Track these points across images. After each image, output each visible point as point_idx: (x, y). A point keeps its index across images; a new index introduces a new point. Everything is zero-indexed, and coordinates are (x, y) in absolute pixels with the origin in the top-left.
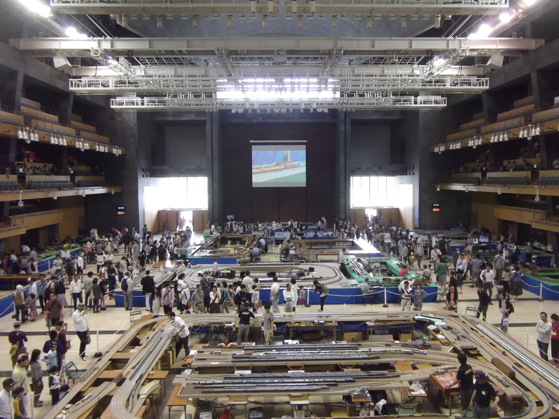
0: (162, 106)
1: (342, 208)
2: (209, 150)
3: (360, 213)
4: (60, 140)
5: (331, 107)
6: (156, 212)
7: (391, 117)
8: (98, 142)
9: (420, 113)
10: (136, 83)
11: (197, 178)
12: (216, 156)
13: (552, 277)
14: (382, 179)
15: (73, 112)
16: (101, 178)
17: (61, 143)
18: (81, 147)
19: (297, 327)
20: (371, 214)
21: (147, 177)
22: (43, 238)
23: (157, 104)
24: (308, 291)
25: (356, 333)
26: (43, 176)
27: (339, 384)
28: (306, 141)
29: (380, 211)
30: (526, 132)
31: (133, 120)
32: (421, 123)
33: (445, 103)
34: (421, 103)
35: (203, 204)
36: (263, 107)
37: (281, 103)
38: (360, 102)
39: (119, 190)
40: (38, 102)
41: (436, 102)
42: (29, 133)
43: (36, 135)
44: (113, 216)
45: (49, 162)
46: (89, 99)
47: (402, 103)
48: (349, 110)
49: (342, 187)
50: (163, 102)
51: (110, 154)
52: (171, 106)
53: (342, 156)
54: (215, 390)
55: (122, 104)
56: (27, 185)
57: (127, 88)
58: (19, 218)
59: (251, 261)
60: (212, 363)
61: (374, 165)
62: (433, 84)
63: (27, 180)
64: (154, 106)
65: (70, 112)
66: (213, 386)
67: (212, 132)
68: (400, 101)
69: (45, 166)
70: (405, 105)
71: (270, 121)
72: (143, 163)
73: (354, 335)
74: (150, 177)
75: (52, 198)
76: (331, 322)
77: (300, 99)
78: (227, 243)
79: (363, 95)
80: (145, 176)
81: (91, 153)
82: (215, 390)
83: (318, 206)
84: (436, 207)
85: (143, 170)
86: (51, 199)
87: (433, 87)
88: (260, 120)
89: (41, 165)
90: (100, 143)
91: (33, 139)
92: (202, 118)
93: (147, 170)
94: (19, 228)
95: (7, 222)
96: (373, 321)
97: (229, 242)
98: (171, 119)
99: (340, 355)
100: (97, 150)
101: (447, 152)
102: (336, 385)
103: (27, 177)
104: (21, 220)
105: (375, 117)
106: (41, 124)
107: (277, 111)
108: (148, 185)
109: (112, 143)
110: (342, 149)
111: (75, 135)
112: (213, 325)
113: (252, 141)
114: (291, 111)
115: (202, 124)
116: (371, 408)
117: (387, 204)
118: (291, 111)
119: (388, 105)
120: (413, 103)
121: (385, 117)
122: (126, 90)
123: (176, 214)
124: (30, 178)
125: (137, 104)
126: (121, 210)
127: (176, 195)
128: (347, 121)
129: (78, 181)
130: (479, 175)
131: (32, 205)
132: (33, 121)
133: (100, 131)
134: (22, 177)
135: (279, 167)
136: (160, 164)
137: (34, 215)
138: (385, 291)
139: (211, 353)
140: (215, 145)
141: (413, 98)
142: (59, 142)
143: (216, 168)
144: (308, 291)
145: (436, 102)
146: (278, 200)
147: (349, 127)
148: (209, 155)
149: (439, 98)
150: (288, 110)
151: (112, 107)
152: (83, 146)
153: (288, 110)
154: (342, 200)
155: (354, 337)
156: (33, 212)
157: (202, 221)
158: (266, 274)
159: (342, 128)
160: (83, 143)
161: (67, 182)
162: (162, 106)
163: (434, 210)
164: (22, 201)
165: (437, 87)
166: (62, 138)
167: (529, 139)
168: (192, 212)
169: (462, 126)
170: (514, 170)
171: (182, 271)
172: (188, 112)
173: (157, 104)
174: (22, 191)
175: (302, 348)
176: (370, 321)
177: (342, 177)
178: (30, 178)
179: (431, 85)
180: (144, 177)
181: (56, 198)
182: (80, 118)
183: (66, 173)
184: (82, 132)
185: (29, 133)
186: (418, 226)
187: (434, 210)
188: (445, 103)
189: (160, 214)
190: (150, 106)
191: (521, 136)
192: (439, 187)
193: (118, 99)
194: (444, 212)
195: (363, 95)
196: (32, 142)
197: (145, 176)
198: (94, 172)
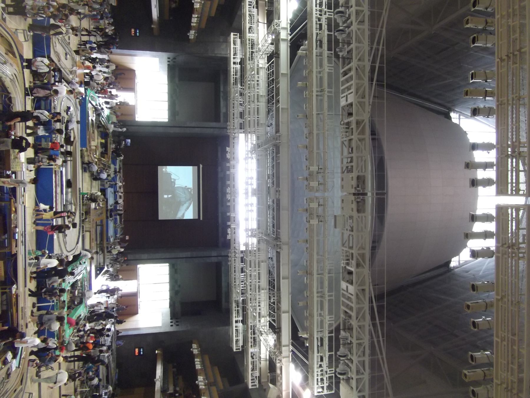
0: (232, 81)
1: (137, 256)
2: (193, 124)
5: (232, 242)
7: (223, 300)
8: (201, 17)
12: (188, 131)
19: (10, 209)
28: (201, 219)
32: (218, 328)
34: (236, 327)
39: (156, 32)
41: (237, 341)
46: (238, 13)
50: (236, 83)
51: (189, 28)
52: (232, 90)
55: (235, 44)
62: (253, 336)
64: (232, 73)
68: (238, 307)
70: (234, 312)
72: (181, 58)
74: (168, 65)
76: (16, 246)
80: (169, 60)
83: (142, 233)
84: (139, 352)
85: (175, 58)
90: (200, 18)
93: (174, 62)
97: (103, 141)
98: (222, 89)
100: (193, 16)
101: (192, 357)
105: (224, 284)
108: (160, 62)
109: (200, 31)
110: (195, 254)
113: (201, 166)
120: (237, 319)
123: (130, 87)
126: (135, 33)
127: (149, 90)
128: (220, 258)
133: (210, 20)
136: (180, 76)
141: (240, 319)
143: (177, 130)
145: (237, 341)
146: (143, 190)
147: (214, 260)
148: (188, 124)
149: (241, 343)
151: (232, 34)
154: (145, 256)
158: (69, 178)
159: (214, 253)
163: (137, 350)
165: (250, 340)
168: (134, 104)
172: (227, 106)
176: (17, 289)
177: (168, 255)
180: (169, 58)
186: (120, 334)
187: (137, 350)
190: (232, 70)
193: (238, 41)
197: (169, 60)
198: (172, 11)
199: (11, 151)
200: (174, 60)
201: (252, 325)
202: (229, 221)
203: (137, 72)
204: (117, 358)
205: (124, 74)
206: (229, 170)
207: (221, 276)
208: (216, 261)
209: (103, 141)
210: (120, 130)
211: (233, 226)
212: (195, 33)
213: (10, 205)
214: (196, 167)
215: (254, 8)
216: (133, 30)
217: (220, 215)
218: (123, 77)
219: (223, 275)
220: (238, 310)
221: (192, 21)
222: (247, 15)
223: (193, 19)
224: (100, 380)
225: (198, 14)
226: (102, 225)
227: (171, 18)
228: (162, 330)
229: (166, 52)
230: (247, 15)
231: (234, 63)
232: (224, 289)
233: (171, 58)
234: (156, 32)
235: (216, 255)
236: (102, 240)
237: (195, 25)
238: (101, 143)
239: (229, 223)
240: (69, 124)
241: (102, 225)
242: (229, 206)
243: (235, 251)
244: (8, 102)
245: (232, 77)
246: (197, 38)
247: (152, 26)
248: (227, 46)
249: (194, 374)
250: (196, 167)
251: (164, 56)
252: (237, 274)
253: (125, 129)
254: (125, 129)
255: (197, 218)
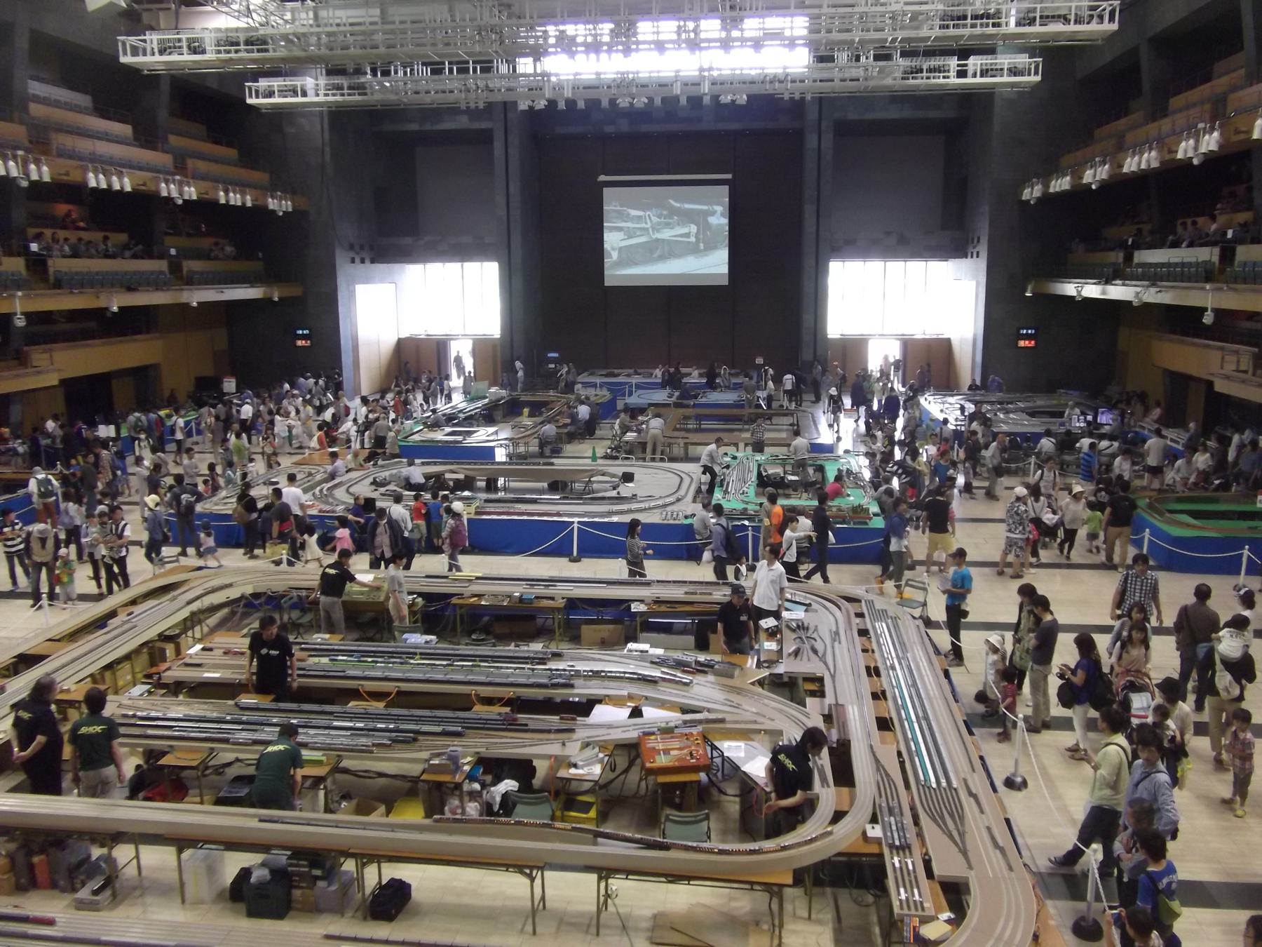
0: (357, 98)
1: (806, 337)
2: (501, 199)
3: (853, 348)
4: (115, 178)
5: (756, 90)
6: (395, 340)
7: (933, 114)
8: (224, 182)
9: (998, 103)
10: (265, 42)
11: (847, 264)
12: (516, 214)
13: (1196, 515)
14: (916, 267)
15: (172, 114)
16: (256, 266)
17: (117, 187)
18: (175, 194)
19: (472, 606)
20: (880, 355)
21: (363, 261)
22: (122, 392)
23: (346, 91)
24: (576, 525)
25: (611, 627)
26: (100, 261)
27: (420, 738)
28: (729, 176)
29: (908, 345)
30: (1191, 142)
31: (318, 134)
32: (997, 128)
33: (1036, 73)
34: (975, 75)
35: (490, 323)
36: (592, 95)
37: (624, 84)
38: (825, 75)
39: (293, 291)
40: (86, 93)
41: (1014, 71)
42: (25, 164)
43: (45, 169)
44: (286, 344)
45: (118, 229)
46: (213, 84)
47: (925, 74)
48: (797, 96)
49: (807, 287)
50: (361, 88)
51: (260, 211)
52: (378, 97)
53: (809, 210)
54: (150, 732)
55: (270, 94)
56: (52, 279)
57: (243, 55)
58: (45, 352)
59: (542, 455)
60: (206, 675)
61: (888, 234)
62: (969, 21)
63: (51, 270)
64: (338, 98)
65: (163, 114)
66: (132, 721)
67: (507, 153)
68: (921, 71)
69: (106, 238)
70: (933, 81)
71: (645, 128)
72: (347, 230)
73: (606, 630)
74: (372, 262)
75: (187, 304)
76: (552, 599)
77: (598, 74)
78: (521, 414)
79: (831, 59)
80: (357, 260)
81: (204, 209)
82: (150, 732)
83: (755, 329)
84: (1027, 337)
85: (352, 247)
86: (186, 306)
87: (967, 32)
88: (624, 126)
89: (96, 236)
90: (228, 184)
91: (35, 177)
92: (484, 125)
93: (362, 247)
94: (39, 373)
95: (21, 360)
96: (649, 600)
97: (526, 411)
98: (414, 127)
99: (529, 677)
100: (223, 201)
101: (1047, 200)
102: (415, 740)
103: (50, 262)
104: (46, 356)
105: (894, 113)
106: (69, 142)
107: (623, 103)
108: (367, 281)
109: (277, 185)
110: (809, 193)
111: (172, 170)
112: (295, 593)
113: (602, 178)
114: (658, 102)
115: (485, 138)
116: (473, 795)
117: (926, 328)
118: (658, 102)
119: (889, 81)
120: (953, 74)
121: (920, 114)
122: (231, 59)
123: (440, 347)
124: (58, 264)
125: (304, 94)
126: (304, 337)
127: (433, 302)
128: (824, 124)
129: (189, 271)
130: (1119, 256)
131: (92, 325)
132: (53, 136)
133: (249, 159)
134: (37, 265)
135: (666, 239)
136: (396, 234)
137: (1197, 345)
138: (750, 533)
139: (225, 653)
140: (514, 189)
141: (953, 62)
142: (110, 185)
144: (576, 525)
145: (1014, 71)
147: (828, 141)
148: (502, 212)
149: (1023, 60)
150: (651, 100)
151: (249, 101)
152: (181, 194)
153: (651, 100)
154: (807, 318)
155: (605, 635)
156: (84, 339)
157: (495, 360)
158: (545, 485)
159: (811, 141)
160: (181, 185)
161: (162, 273)
162: (357, 98)
163: (1022, 343)
164: (22, 314)
165: (978, 30)
166: (121, 175)
167: (1195, 162)
168: (471, 342)
169: (1097, 132)
170: (1191, 245)
171: (988, 470)
172: (453, 111)
173: (346, 91)
174: (20, 294)
175: (415, 654)
176: (642, 601)
177: (809, 262)
178: (58, 264)
179: (965, 26)
180: (353, 261)
181: (195, 304)
182: (200, 129)
183: (162, 255)
184: (190, 163)
185: (25, 164)
186: (978, 383)
187: (1022, 343)
188: (1036, 73)
189: (402, 346)
190: (330, 98)
191: (1180, 156)
192: (1030, 288)
193: (263, 83)
194: (1041, 348)
195: (831, 59)
196: (33, 183)
197: (357, 260)
198: (244, 252)
199: (344, 598)
200: (357, 248)
201: (938, 22)
202: (598, 102)
203: (404, 334)
204: (1023, 392)
205: (406, 363)
206: (676, 99)
207: (873, 122)
208: (831, 136)
209: (526, 411)
210: (520, 374)
211: (568, 94)
212: (273, 197)
213: (461, 606)
214: (607, 191)
215: (145, 41)
216: (299, 343)
217: (721, 126)
218: (416, 365)
219: (869, 116)
220: (930, 70)
221: (239, 204)
222: (165, 58)
223: (232, 203)
224: (1048, 433)
225: (217, 190)
226: (699, 418)
227: (260, 255)
228: (983, 279)
229: (333, 267)
230: (165, 58)
231: (962, 74)
232: (905, 113)
233: (352, 254)
234: (293, 291)
235: (815, 137)
236: (737, 419)
237: (248, 197)
238: (531, 415)
239: (562, 105)
240: (413, 481)
241: (699, 418)
242: (586, 101)
243: (771, 82)
244: (263, 600)
245: (347, 98)
246: (290, 190)
247: (115, 309)
248: (304, 115)
249: (1079, 194)
250: (607, 191)
251: (345, 270)
252: (836, 74)
253: (518, 364)
254: (518, 364)
255: (726, 188)
